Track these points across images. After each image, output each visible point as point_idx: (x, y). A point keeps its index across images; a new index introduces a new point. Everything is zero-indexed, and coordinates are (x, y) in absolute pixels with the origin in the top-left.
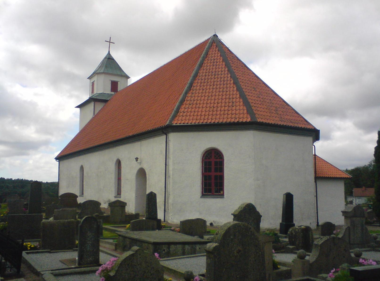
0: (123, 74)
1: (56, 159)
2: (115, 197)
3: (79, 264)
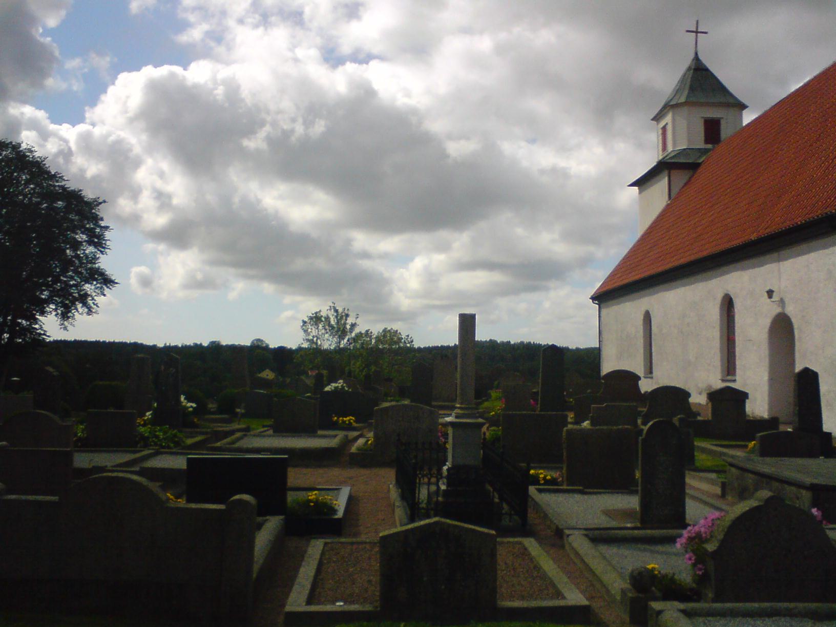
0: (731, 101)
1: (594, 298)
2: (723, 381)
3: (643, 521)
